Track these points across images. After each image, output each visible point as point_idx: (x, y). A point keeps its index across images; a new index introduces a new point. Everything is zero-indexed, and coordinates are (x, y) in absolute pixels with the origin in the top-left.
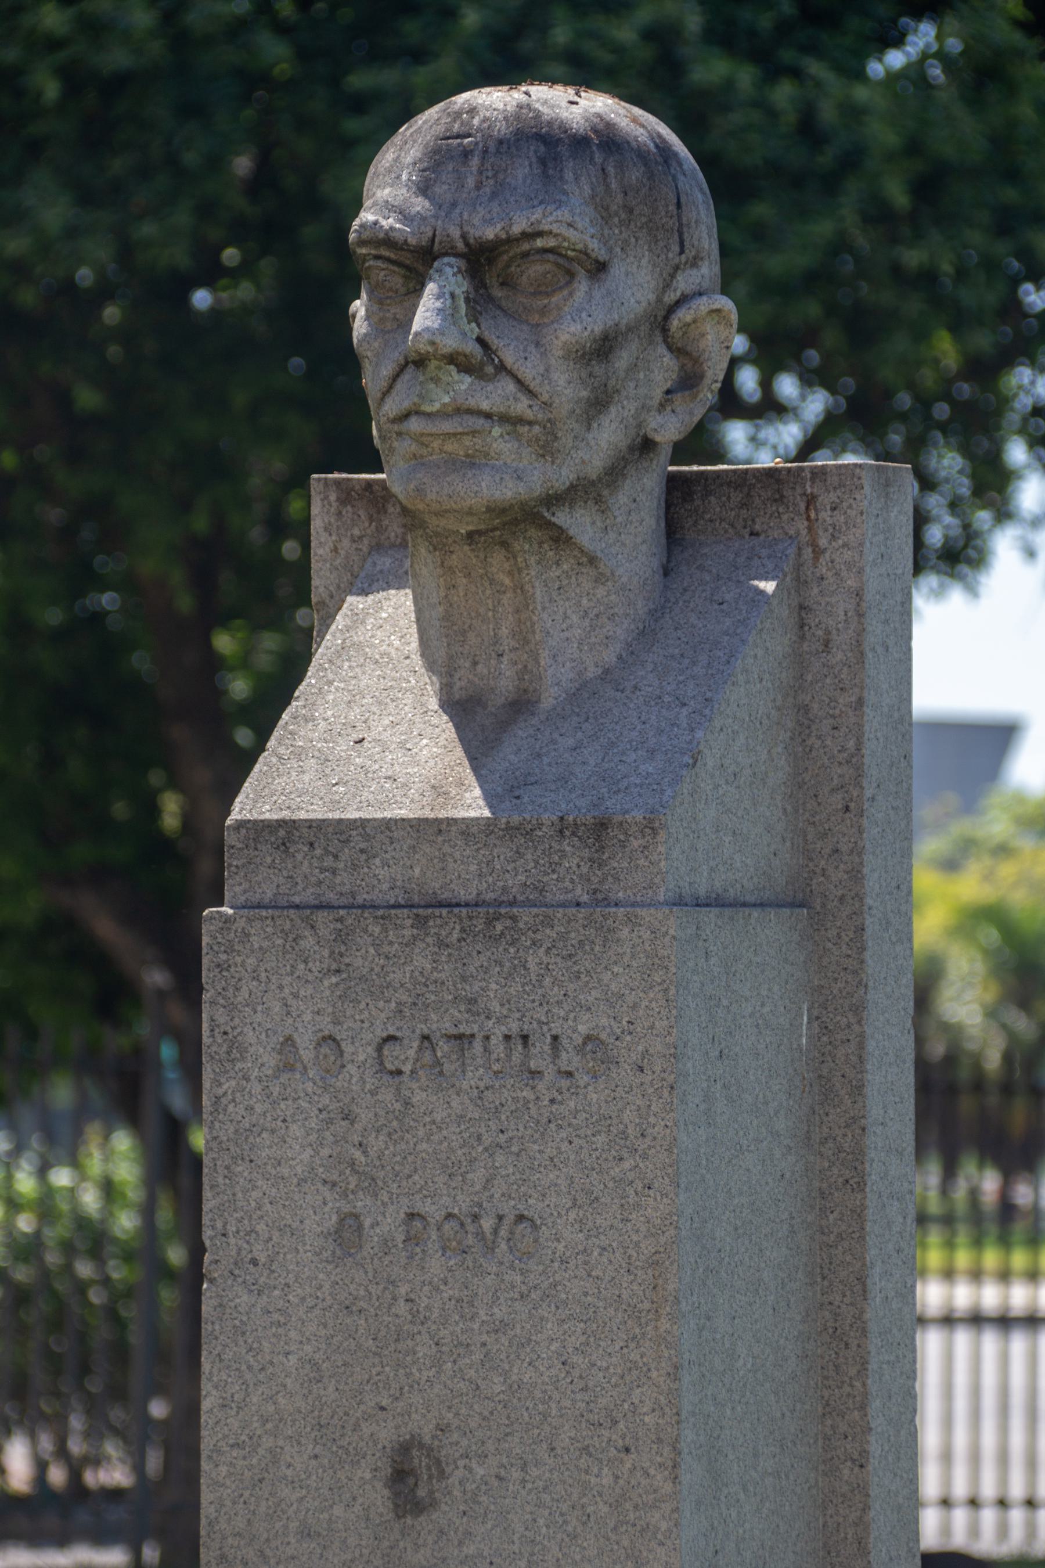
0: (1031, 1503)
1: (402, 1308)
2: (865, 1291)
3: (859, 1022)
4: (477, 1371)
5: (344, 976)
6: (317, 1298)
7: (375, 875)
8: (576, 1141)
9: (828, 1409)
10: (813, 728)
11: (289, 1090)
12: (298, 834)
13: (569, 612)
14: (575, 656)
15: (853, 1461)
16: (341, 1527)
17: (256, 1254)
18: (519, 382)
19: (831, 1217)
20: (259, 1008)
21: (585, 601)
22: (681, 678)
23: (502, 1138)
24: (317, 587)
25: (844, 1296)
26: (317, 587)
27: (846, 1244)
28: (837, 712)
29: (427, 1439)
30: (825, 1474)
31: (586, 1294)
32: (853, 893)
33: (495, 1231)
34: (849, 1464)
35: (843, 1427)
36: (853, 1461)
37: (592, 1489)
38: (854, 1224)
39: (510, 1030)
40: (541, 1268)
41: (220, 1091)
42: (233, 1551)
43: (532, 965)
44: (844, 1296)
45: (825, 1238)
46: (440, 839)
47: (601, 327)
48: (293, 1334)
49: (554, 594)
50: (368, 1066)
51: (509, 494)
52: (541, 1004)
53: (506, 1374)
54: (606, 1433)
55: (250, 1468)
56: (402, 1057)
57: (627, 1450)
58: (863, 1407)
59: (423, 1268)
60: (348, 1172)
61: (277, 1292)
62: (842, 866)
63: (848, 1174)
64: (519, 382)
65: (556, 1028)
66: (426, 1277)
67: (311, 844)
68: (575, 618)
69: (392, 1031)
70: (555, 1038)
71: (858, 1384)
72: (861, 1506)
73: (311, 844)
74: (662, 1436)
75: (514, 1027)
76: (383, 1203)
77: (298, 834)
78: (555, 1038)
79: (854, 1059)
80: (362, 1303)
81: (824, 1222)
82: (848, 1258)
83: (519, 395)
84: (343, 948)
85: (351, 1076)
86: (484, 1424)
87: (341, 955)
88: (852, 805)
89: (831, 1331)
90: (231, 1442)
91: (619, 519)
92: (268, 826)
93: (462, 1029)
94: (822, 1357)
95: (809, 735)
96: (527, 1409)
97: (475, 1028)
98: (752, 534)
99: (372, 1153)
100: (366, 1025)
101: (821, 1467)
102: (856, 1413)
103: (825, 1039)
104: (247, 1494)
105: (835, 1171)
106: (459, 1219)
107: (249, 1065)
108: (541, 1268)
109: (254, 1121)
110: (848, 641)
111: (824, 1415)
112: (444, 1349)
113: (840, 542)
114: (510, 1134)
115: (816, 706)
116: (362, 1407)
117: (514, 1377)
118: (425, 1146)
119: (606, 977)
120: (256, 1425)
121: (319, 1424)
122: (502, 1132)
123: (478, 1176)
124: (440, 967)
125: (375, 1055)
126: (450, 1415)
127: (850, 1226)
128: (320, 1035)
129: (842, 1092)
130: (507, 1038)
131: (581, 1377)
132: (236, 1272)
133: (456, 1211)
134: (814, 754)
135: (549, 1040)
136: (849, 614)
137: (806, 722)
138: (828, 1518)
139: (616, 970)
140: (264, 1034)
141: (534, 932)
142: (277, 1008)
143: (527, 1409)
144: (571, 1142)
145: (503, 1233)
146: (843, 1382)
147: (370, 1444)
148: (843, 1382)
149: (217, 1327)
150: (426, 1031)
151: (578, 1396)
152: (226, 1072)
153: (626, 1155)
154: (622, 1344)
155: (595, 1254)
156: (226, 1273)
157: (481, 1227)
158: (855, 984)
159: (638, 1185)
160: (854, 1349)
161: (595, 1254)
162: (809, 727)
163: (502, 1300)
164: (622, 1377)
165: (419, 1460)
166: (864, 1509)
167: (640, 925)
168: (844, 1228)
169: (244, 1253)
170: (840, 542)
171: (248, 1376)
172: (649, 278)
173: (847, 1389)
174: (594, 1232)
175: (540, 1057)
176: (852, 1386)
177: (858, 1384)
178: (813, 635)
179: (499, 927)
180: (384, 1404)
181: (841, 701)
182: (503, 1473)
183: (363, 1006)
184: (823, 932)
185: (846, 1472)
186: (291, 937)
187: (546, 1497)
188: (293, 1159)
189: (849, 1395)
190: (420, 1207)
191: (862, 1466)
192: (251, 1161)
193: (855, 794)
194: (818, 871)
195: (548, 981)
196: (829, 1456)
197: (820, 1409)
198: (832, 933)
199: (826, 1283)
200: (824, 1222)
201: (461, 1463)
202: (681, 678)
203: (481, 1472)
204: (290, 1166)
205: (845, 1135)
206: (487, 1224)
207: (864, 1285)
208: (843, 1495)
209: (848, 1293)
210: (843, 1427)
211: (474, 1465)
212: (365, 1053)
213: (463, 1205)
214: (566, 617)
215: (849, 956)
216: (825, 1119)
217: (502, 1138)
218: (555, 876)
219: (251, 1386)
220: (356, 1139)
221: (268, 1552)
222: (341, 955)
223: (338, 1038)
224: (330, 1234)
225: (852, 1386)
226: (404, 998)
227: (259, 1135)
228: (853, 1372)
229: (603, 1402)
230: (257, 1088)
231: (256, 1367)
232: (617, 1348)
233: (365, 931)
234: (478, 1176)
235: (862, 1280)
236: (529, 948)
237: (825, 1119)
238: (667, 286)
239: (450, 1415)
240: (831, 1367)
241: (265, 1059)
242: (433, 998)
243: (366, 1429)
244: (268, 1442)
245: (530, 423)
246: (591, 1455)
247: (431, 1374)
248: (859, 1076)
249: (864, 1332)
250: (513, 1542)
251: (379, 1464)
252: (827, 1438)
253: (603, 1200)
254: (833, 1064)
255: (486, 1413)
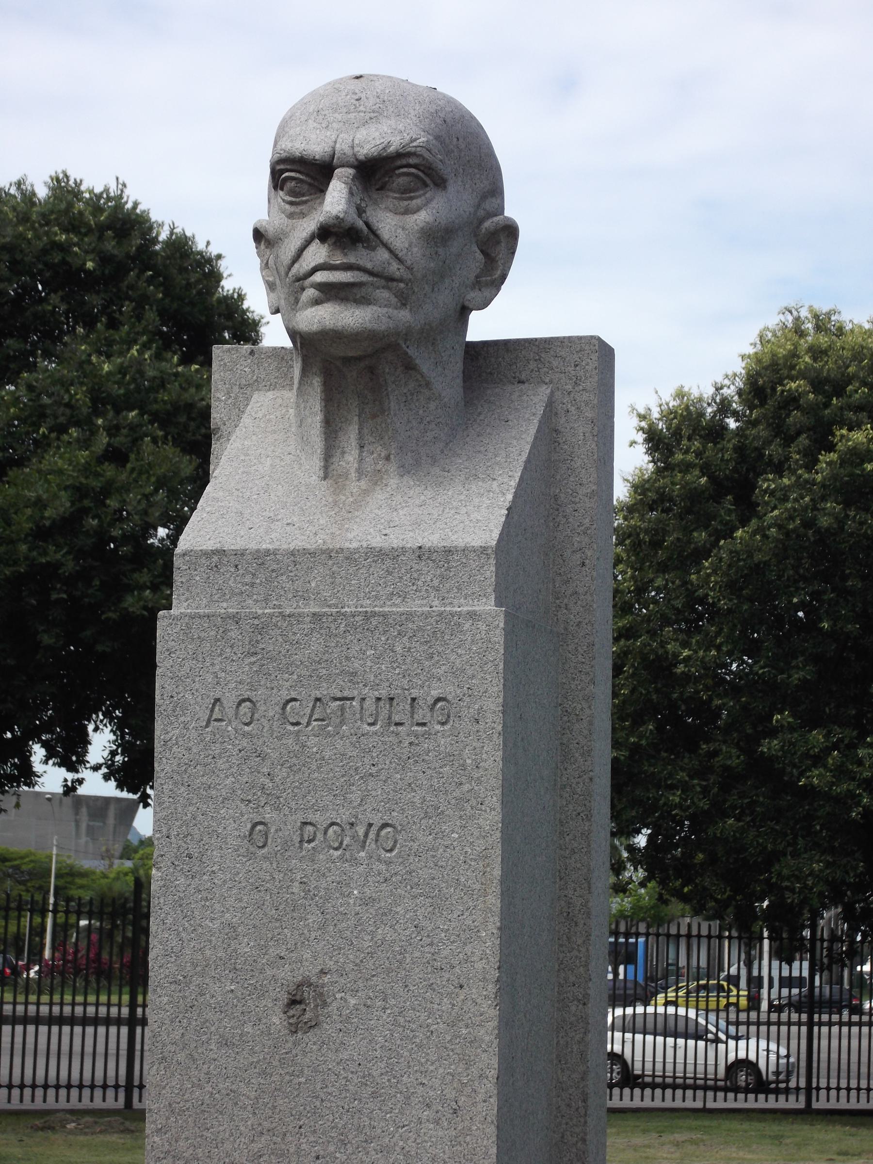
0: (10, 1087)
1: (296, 888)
2: (590, 888)
3: (590, 707)
4: (352, 932)
5: (260, 656)
6: (235, 881)
7: (282, 587)
8: (429, 772)
9: (562, 966)
10: (560, 510)
11: (218, 736)
12: (226, 559)
13: (411, 418)
14: (414, 448)
15: (579, 1001)
16: (250, 1039)
17: (191, 851)
18: (391, 251)
19: (567, 838)
20: (197, 679)
21: (421, 412)
22: (489, 464)
23: (374, 770)
24: (214, 419)
25: (575, 891)
26: (214, 419)
27: (577, 856)
28: (577, 500)
29: (314, 979)
30: (559, 1009)
31: (433, 879)
32: (587, 621)
33: (366, 835)
34: (575, 1002)
35: (572, 979)
36: (579, 1001)
37: (435, 1013)
38: (583, 842)
39: (380, 694)
40: (400, 860)
41: (168, 737)
42: (171, 1055)
43: (398, 649)
44: (575, 891)
45: (562, 852)
46: (330, 562)
47: (346, 313)
48: (217, 906)
49: (402, 405)
50: (275, 719)
51: (383, 327)
52: (404, 676)
53: (373, 934)
54: (447, 975)
55: (184, 997)
56: (302, 713)
57: (461, 987)
58: (586, 965)
59: (313, 860)
60: (259, 793)
61: (205, 877)
62: (579, 602)
63: (579, 809)
64: (391, 251)
65: (415, 693)
66: (315, 866)
67: (236, 566)
68: (414, 423)
69: (293, 695)
70: (413, 700)
71: (583, 950)
72: (583, 1030)
73: (236, 566)
74: (487, 976)
75: (383, 693)
76: (285, 815)
77: (226, 559)
78: (413, 700)
79: (586, 732)
80: (268, 885)
81: (561, 842)
82: (579, 865)
83: (391, 261)
84: (259, 637)
85: (264, 727)
86: (356, 968)
87: (257, 642)
88: (587, 562)
89: (565, 914)
90: (170, 980)
91: (444, 359)
92: (205, 554)
93: (346, 694)
94: (559, 932)
95: (558, 515)
96: (388, 958)
97: (356, 693)
98: (519, 382)
99: (277, 779)
100: (275, 691)
101: (556, 1005)
102: (582, 968)
103: (566, 718)
104: (181, 1016)
105: (571, 807)
106: (341, 826)
107: (189, 719)
108: (400, 860)
109: (192, 757)
110: (586, 453)
111: (559, 970)
112: (328, 916)
113: (581, 387)
114: (380, 767)
115: (562, 495)
116: (266, 957)
117: (379, 937)
118: (316, 774)
119: (453, 657)
120: (189, 969)
121: (235, 968)
122: (374, 765)
123: (355, 797)
124: (330, 651)
125: (280, 711)
126: (332, 963)
127: (580, 844)
128: (241, 698)
129: (577, 755)
130: (379, 699)
131: (428, 936)
132: (176, 863)
133: (338, 821)
134: (561, 527)
135: (409, 701)
136: (587, 435)
137: (556, 507)
138: (560, 1038)
139: (459, 651)
140: (200, 697)
141: (400, 626)
142: (210, 678)
143: (388, 958)
144: (424, 772)
145: (372, 835)
146: (573, 949)
147: (272, 982)
148: (573, 949)
149: (162, 901)
150: (319, 696)
151: (427, 949)
152: (172, 723)
153: (464, 781)
154: (459, 913)
155: (441, 850)
156: (169, 863)
157: (356, 832)
158: (587, 681)
159: (473, 802)
160: (581, 926)
161: (441, 850)
162: (558, 510)
163: (371, 883)
164: (458, 936)
165: (308, 994)
166: (585, 1033)
167: (479, 621)
168: (576, 845)
169: (182, 850)
170: (581, 387)
171: (183, 935)
172: (470, 197)
173: (575, 953)
174: (440, 835)
175: (401, 712)
176: (579, 951)
177: (583, 950)
178: (562, 449)
179: (374, 623)
180: (282, 954)
181: (580, 492)
182: (369, 1002)
183: (273, 677)
184: (565, 647)
185: (573, 1008)
186: (221, 630)
187: (401, 1020)
188: (219, 785)
189: (576, 957)
190: (311, 818)
191: (584, 1004)
192: (189, 786)
193: (589, 555)
194: (563, 605)
195: (409, 660)
196: (562, 997)
197: (557, 966)
198: (571, 647)
199: (562, 882)
200: (561, 842)
201: (338, 996)
202: (489, 464)
203: (353, 1002)
204: (217, 790)
205: (578, 783)
206: (361, 830)
207: (589, 883)
208: (571, 1023)
209: (578, 889)
210: (572, 979)
211: (348, 997)
212: (274, 711)
213: (344, 816)
214: (409, 422)
215: (583, 663)
216: (565, 772)
217: (374, 770)
218: (415, 588)
219: (186, 941)
220: (265, 770)
221: (196, 1056)
222: (257, 642)
223: (254, 700)
224: (245, 837)
225: (579, 951)
226: (304, 672)
227: (195, 768)
228: (580, 942)
229: (445, 953)
230: (194, 734)
231: (190, 929)
232: (455, 916)
233: (276, 625)
234: (355, 797)
235: (588, 881)
236: (396, 637)
237: (565, 772)
238: (478, 206)
239: (332, 963)
240: (565, 937)
241: (201, 715)
242: (324, 671)
243: (269, 972)
244: (197, 980)
245: (401, 280)
246: (434, 990)
247: (318, 934)
248: (589, 743)
249: (588, 914)
250: (376, 1050)
251: (279, 996)
252: (561, 985)
253: (447, 813)
254: (570, 736)
255: (358, 961)
